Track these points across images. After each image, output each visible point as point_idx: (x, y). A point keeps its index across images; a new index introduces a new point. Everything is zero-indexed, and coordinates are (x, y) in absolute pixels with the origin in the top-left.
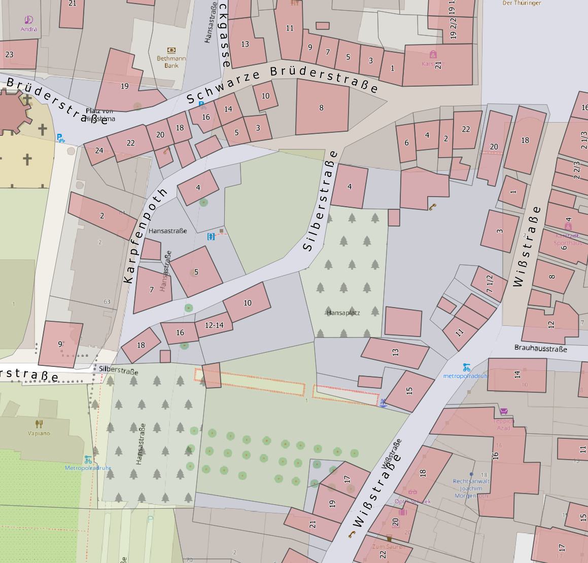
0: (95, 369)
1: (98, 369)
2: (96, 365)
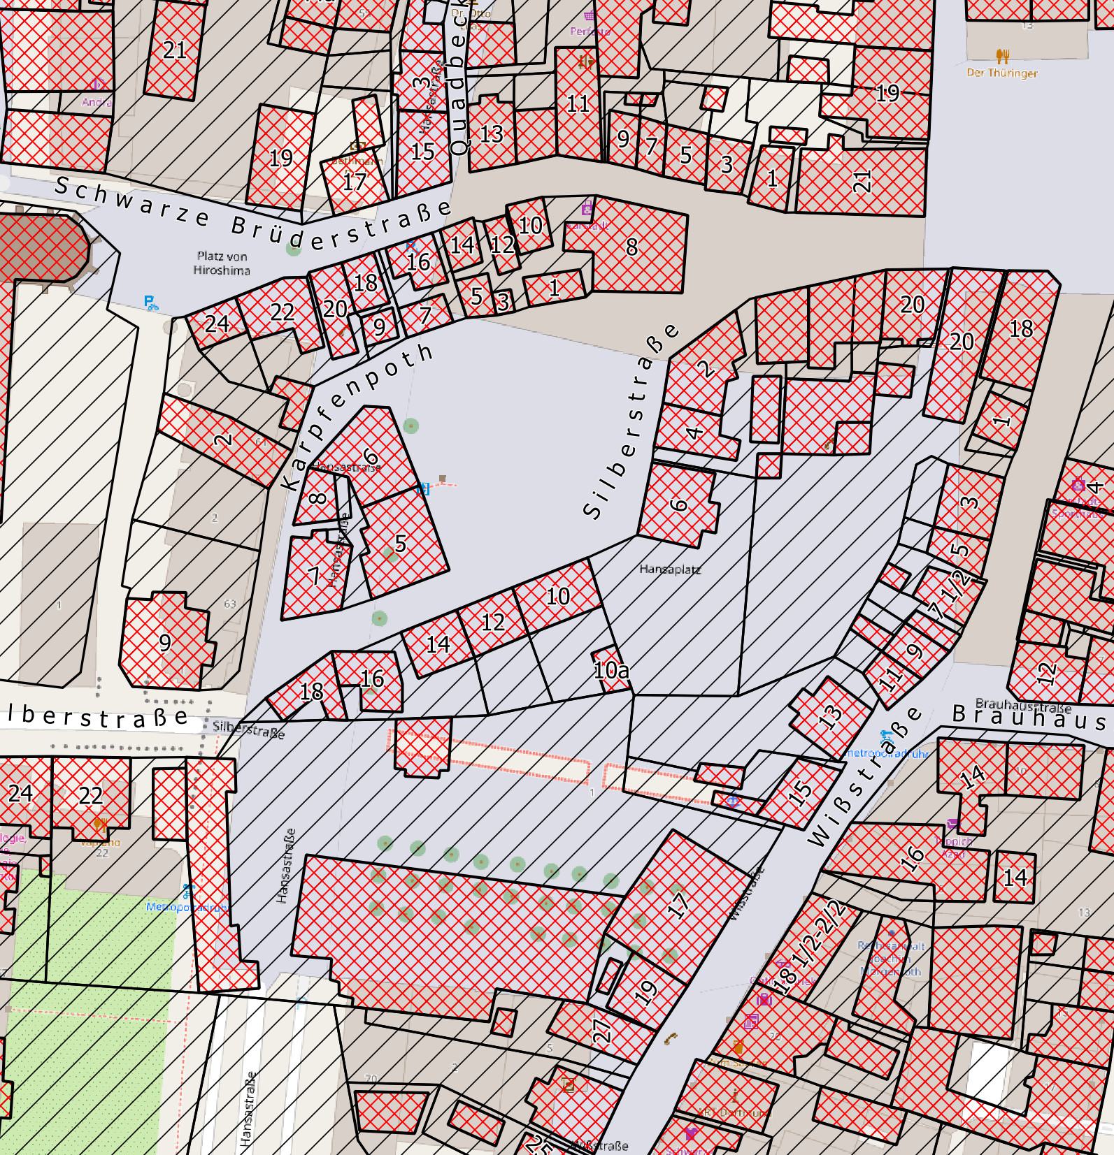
0: (205, 727)
1: (211, 727)
2: (207, 720)
